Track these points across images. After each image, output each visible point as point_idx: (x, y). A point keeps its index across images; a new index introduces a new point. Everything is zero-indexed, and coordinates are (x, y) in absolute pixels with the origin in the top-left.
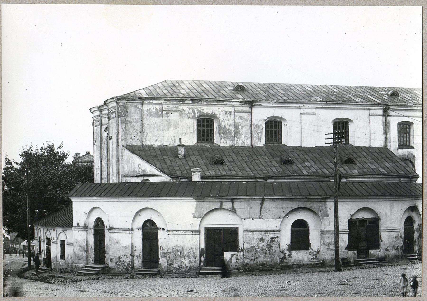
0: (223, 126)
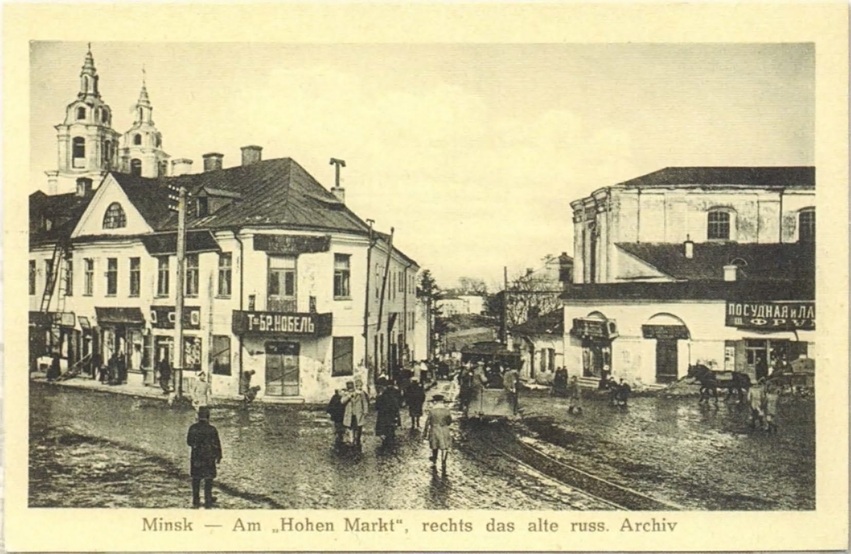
0: (743, 219)
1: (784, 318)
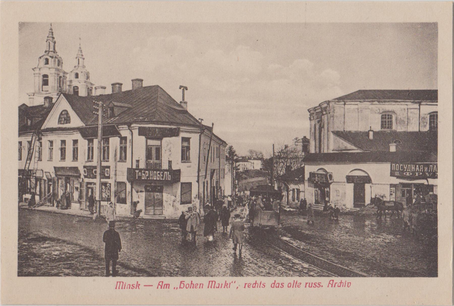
1: (421, 172)
